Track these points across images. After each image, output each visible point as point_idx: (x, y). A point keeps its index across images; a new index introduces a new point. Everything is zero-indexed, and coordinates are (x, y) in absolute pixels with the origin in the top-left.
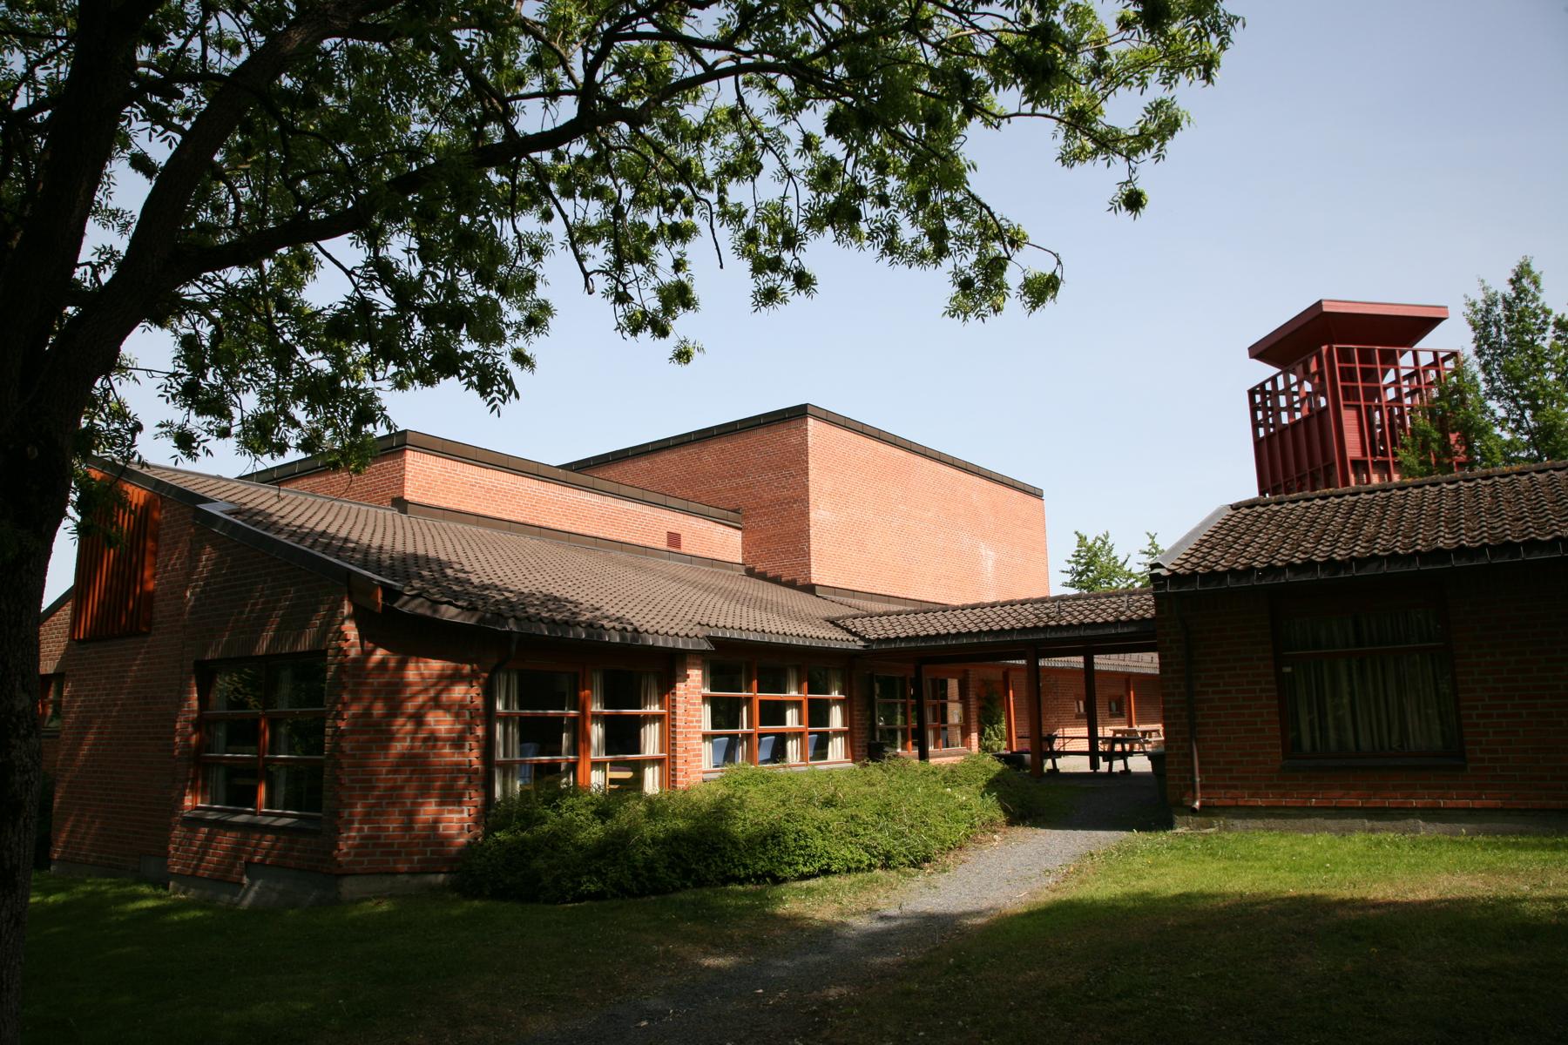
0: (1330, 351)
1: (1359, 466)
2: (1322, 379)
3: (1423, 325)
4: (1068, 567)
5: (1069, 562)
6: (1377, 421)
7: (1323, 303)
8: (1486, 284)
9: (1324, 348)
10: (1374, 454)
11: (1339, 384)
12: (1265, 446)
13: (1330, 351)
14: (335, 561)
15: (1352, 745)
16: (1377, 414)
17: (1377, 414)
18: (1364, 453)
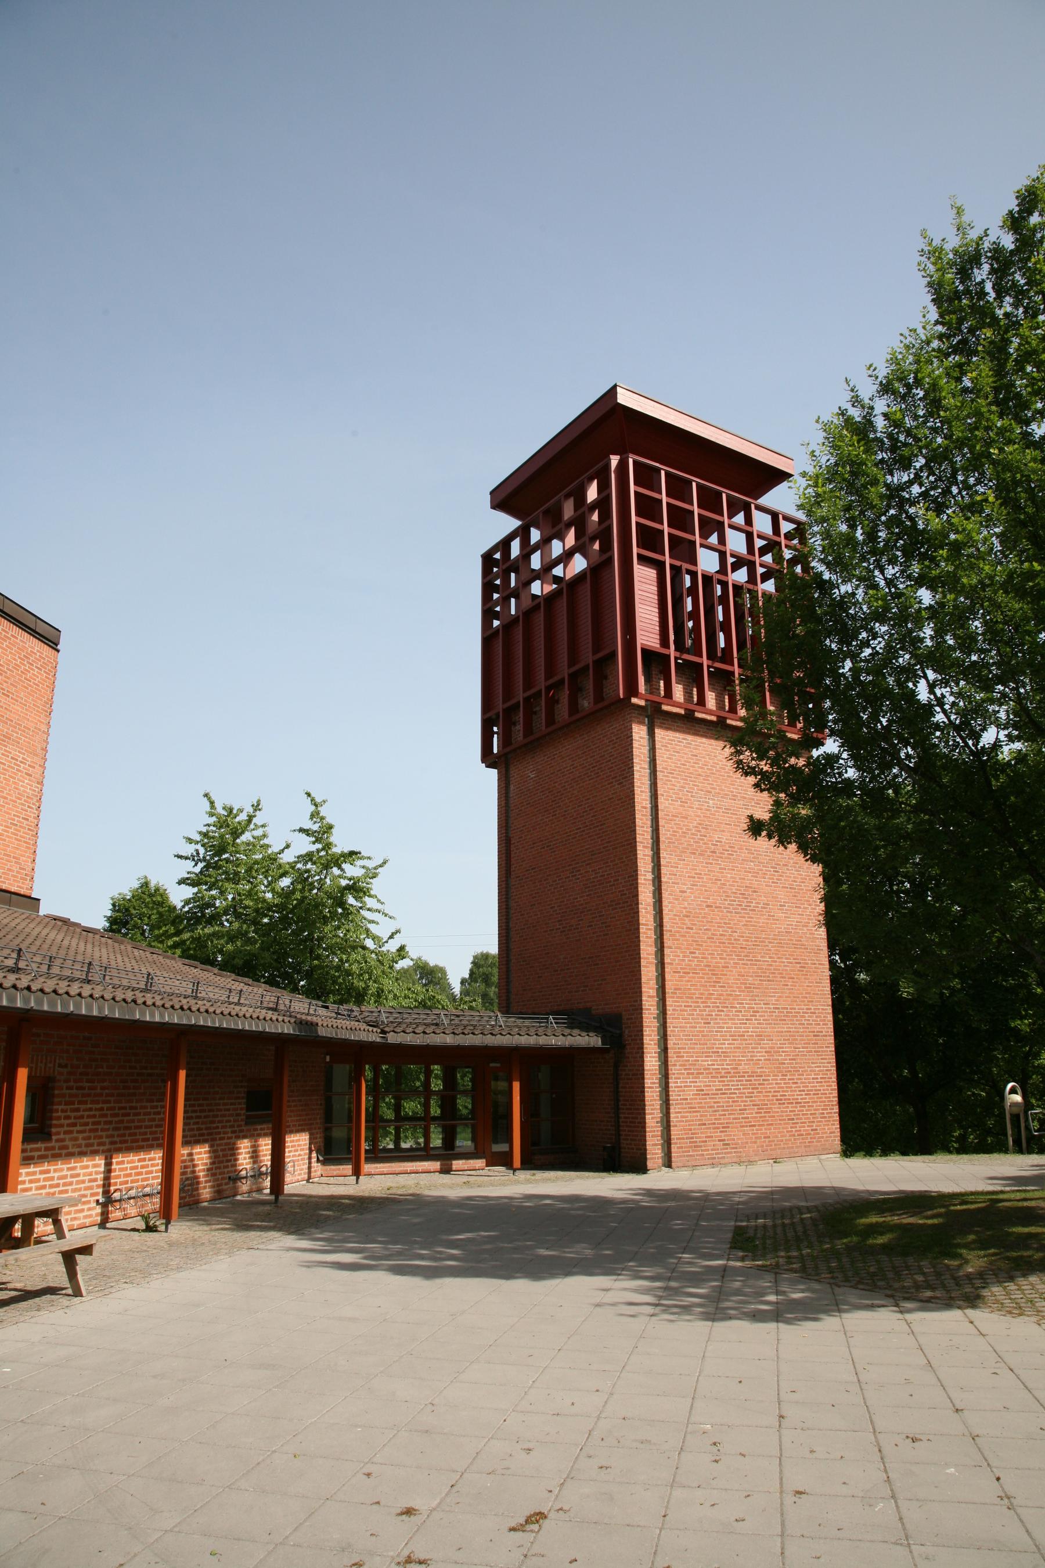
0: (623, 466)
1: (655, 661)
2: (606, 547)
3: (777, 476)
4: (189, 850)
5: (190, 840)
6: (689, 607)
7: (619, 389)
8: (966, 218)
9: (614, 460)
10: (680, 646)
11: (634, 518)
12: (499, 646)
13: (623, 466)
14: (964, 1207)
15: (268, 1208)
16: (689, 601)
17: (689, 601)
18: (664, 641)
